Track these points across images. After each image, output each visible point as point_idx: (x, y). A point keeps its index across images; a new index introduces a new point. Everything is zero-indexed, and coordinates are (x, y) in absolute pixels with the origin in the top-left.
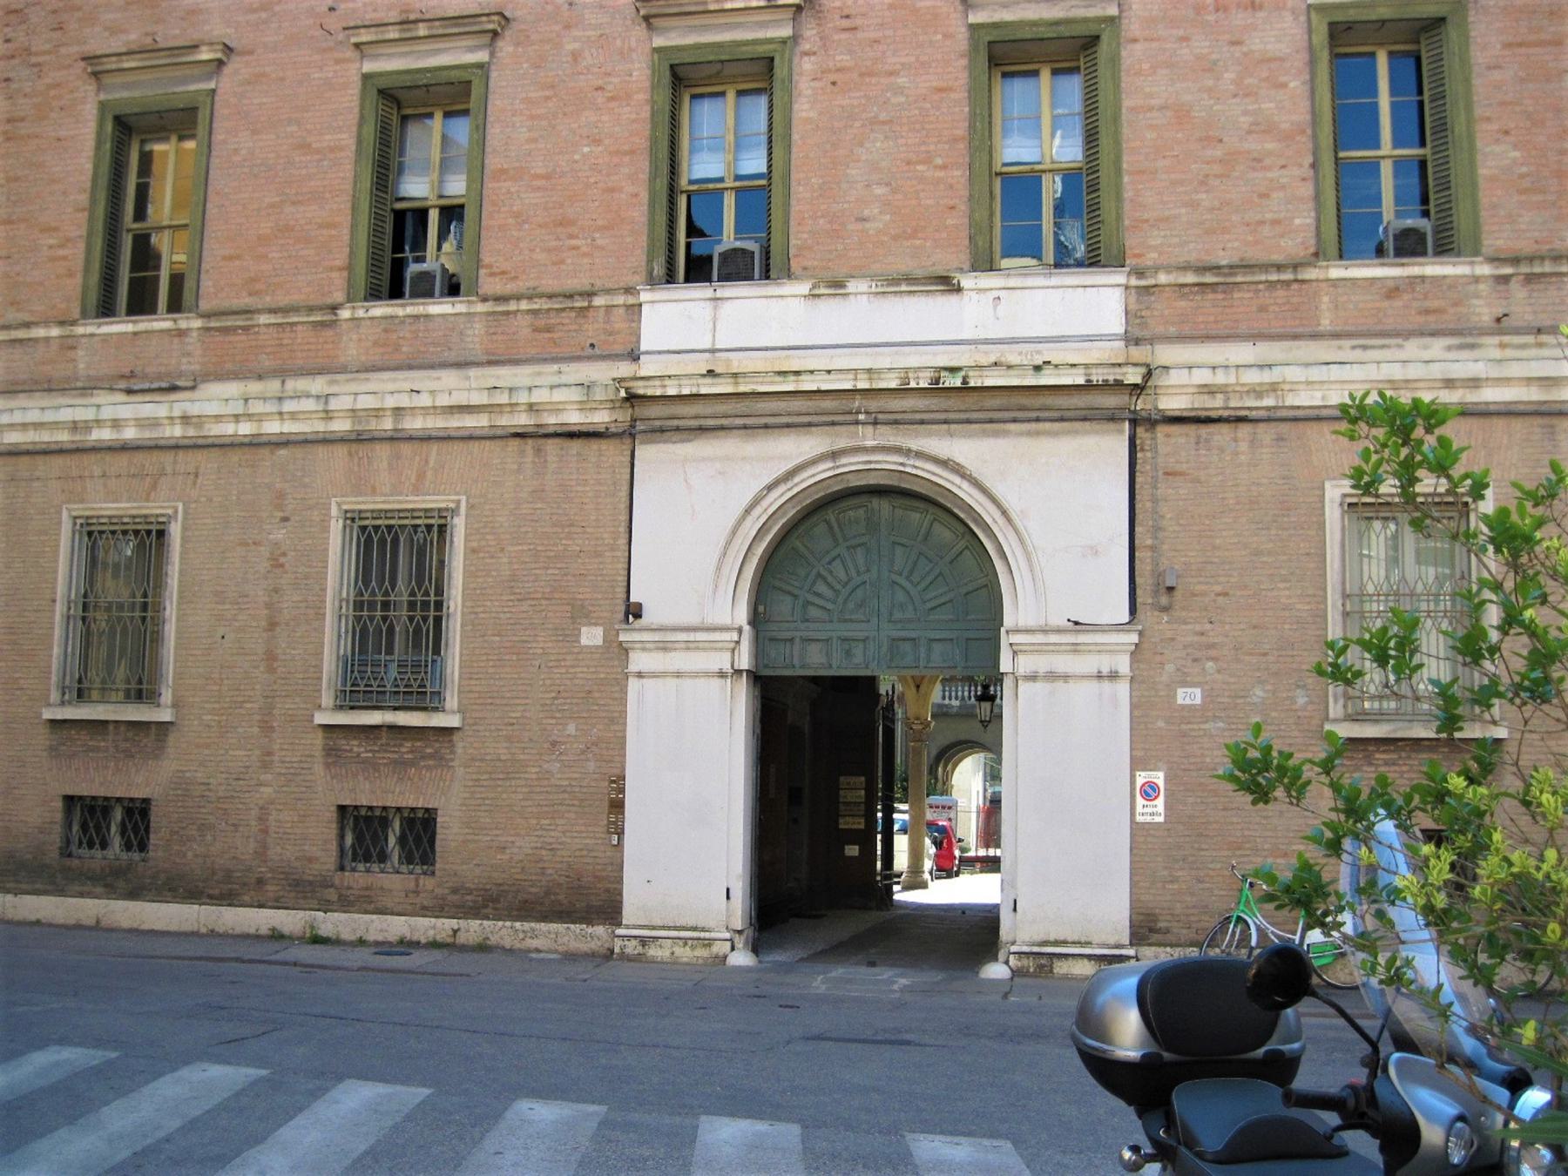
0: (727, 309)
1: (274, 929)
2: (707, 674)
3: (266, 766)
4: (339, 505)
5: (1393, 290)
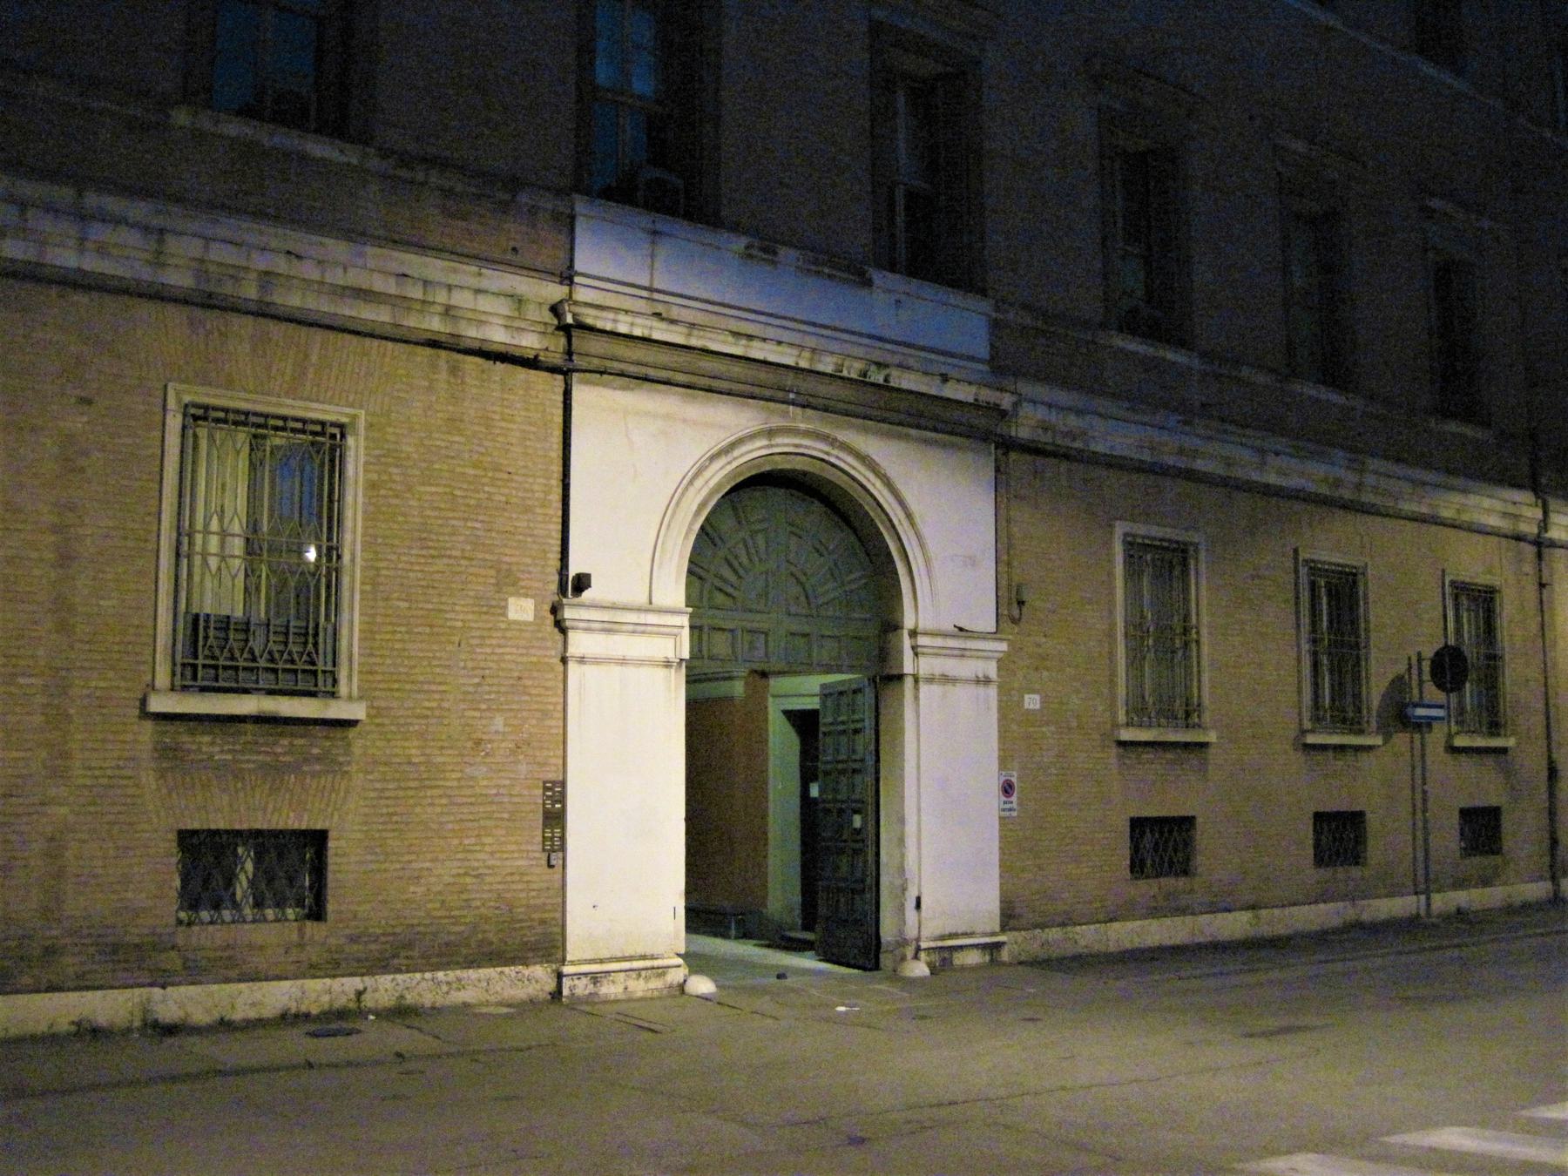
1: (78, 1024)
2: (652, 663)
3: (58, 773)
4: (178, 393)
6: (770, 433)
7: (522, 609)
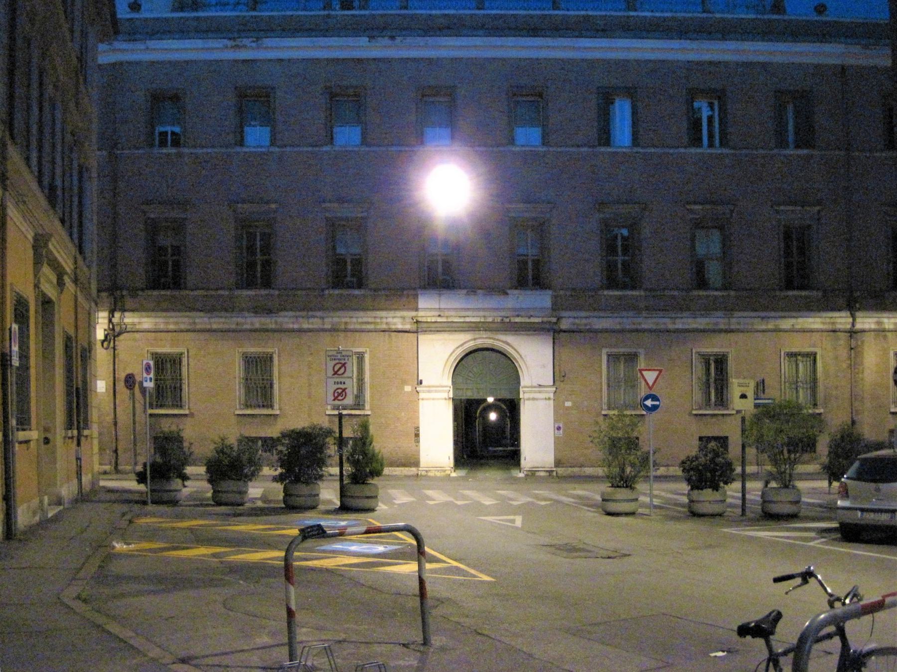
5: (620, 298)
6: (475, 339)
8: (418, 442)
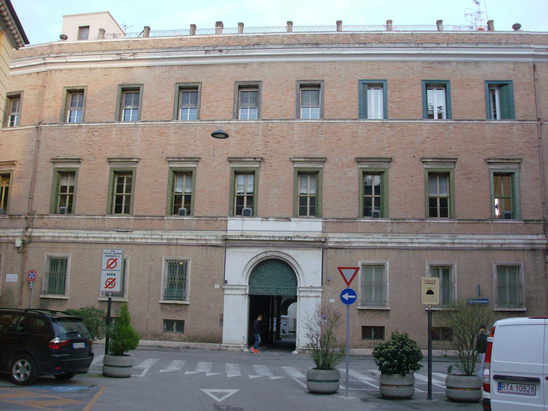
0: (245, 222)
5: (372, 224)
7: (217, 286)
8: (222, 325)
